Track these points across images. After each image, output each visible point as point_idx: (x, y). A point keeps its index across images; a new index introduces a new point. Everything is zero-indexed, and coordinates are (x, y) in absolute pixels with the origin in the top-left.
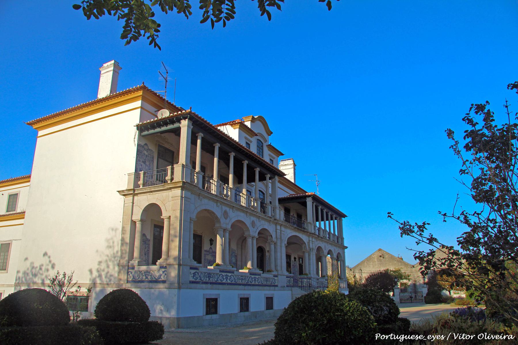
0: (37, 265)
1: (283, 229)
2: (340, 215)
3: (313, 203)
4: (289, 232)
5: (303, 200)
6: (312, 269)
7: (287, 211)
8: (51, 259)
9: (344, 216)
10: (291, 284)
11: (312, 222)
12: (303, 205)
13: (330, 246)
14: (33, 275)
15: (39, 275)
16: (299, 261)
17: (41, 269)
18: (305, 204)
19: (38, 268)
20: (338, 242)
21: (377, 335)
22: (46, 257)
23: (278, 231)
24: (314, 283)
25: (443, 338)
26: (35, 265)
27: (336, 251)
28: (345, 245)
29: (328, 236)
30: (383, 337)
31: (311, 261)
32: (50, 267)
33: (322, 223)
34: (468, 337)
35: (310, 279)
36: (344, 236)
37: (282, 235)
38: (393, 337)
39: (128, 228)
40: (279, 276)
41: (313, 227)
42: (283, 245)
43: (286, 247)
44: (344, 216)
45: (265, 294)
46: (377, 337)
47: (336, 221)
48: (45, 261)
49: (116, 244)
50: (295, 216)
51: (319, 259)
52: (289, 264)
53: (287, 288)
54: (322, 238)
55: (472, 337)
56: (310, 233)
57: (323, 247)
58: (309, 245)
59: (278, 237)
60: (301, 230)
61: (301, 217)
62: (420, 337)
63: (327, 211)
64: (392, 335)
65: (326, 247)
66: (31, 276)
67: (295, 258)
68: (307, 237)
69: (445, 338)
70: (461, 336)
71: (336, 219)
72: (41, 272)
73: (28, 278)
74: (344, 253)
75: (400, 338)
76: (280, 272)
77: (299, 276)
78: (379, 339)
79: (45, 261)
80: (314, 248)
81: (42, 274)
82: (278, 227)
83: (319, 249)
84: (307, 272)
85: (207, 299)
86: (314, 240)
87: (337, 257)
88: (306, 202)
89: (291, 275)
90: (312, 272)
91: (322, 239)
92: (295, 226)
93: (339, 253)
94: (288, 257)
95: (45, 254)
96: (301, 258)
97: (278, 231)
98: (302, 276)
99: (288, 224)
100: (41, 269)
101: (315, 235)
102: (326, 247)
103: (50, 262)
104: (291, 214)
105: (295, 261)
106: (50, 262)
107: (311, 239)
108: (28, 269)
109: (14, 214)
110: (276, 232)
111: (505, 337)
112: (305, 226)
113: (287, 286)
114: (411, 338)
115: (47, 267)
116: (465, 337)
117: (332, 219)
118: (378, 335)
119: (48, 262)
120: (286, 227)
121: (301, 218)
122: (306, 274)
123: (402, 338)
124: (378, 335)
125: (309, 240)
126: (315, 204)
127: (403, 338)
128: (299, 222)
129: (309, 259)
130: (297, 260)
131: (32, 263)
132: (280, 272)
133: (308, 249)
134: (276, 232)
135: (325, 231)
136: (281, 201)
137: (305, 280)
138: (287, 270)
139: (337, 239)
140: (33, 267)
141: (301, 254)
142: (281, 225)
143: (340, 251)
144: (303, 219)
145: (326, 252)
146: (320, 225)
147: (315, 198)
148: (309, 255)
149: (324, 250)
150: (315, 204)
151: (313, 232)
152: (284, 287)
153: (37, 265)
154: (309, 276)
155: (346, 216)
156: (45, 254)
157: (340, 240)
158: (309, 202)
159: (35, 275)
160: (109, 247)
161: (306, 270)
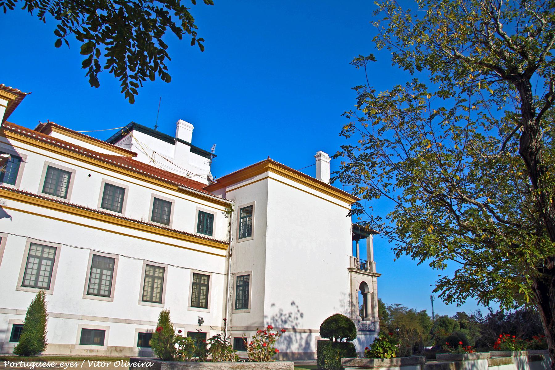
0: (286, 312)
8: (299, 308)
14: (282, 321)
15: (289, 322)
17: (290, 316)
19: (287, 316)
22: (294, 306)
26: (284, 313)
32: (299, 316)
39: (357, 293)
45: (136, 329)
46: (5, 365)
48: (293, 309)
49: (345, 304)
55: (108, 364)
66: (280, 322)
69: (79, 366)
70: (96, 364)
72: (290, 319)
73: (277, 324)
75: (30, 365)
79: (293, 309)
81: (292, 322)
85: (105, 331)
95: (293, 303)
100: (290, 316)
103: (298, 311)
106: (298, 311)
108: (276, 315)
109: (118, 217)
115: (296, 316)
116: (100, 364)
119: (296, 311)
123: (33, 365)
127: (34, 365)
131: (281, 310)
140: (281, 315)
153: (286, 312)
156: (293, 303)
159: (285, 322)
160: (342, 306)
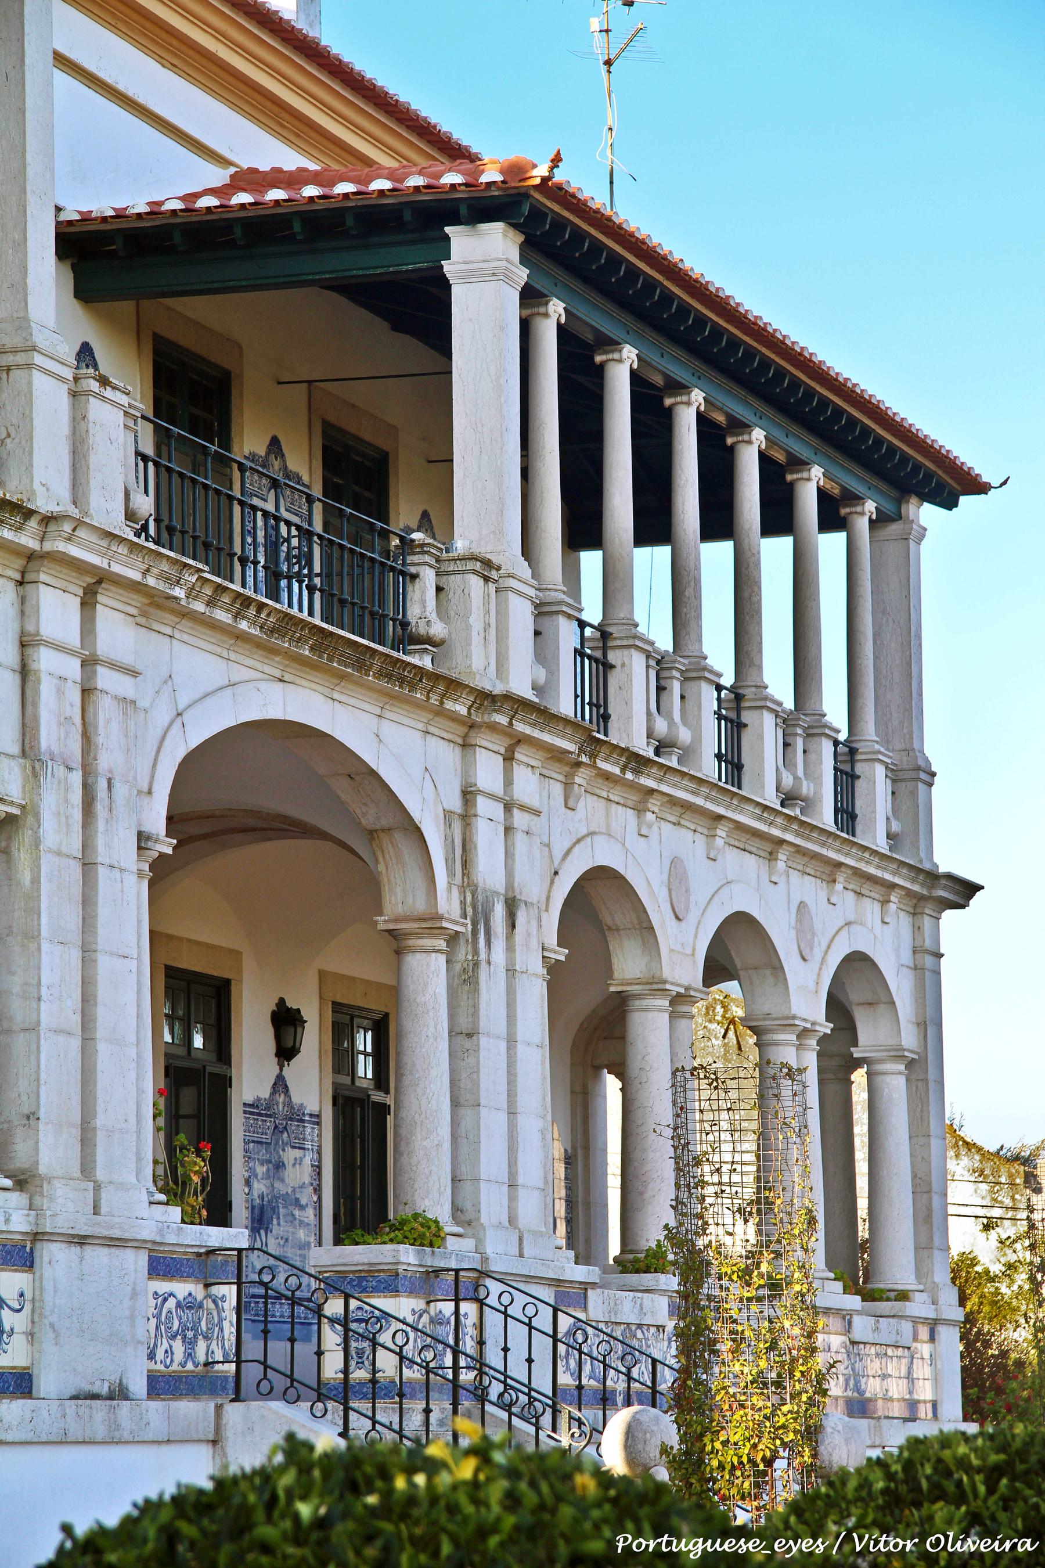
1: (116, 630)
2: (904, 473)
3: (531, 297)
4: (202, 684)
5: (408, 260)
6: (491, 1160)
7: (190, 401)
9: (949, 482)
10: (217, 1349)
11: (508, 552)
12: (399, 324)
13: (745, 865)
16: (343, 1059)
18: (423, 312)
20: (847, 815)
21: (621, 1538)
23: (45, 660)
24: (522, 1355)
25: (822, 1548)
27: (816, 925)
28: (948, 858)
29: (710, 737)
30: (639, 1546)
31: (491, 1052)
33: (652, 564)
34: (896, 1546)
35: (468, 1285)
36: (935, 747)
37: (105, 709)
38: (669, 1544)
40: (55, 1257)
41: (521, 615)
42: (118, 847)
43: (161, 874)
44: (949, 482)
46: (620, 1545)
47: (831, 547)
50: (303, 464)
51: (594, 1037)
52: (194, 1100)
53: (156, 1413)
54: (637, 762)
56: (485, 699)
57: (648, 882)
58: (465, 857)
59: (48, 737)
60: (361, 659)
61: (373, 480)
62: (750, 1545)
63: (728, 413)
64: (666, 1538)
65: (689, 881)
67: (286, 1021)
68: (445, 755)
71: (832, 518)
74: (927, 960)
75: (690, 1547)
76: (65, 1206)
77: (330, 1256)
78: (627, 1549)
80: (531, 884)
82: (57, 609)
83: (598, 905)
84: (436, 1205)
86: (527, 784)
87: (837, 1007)
88: (445, 286)
89: (215, 1236)
90: (491, 1205)
91: (641, 774)
92: (300, 603)
93: (857, 963)
94: (193, 995)
96: (370, 1022)
97: (54, 667)
98: (359, 1255)
99: (187, 582)
101: (546, 716)
102: (689, 881)
104: (249, 442)
105: (286, 1053)
107: (488, 770)
110: (24, 672)
111: (1008, 1545)
112: (421, 605)
113: (160, 1386)
114: (726, 1546)
116: (886, 1543)
117: (779, 518)
118: (626, 1539)
120: (153, 606)
121: (381, 509)
122: (427, 1234)
124: (626, 1539)
125: (468, 795)
126: (557, 308)
128: (352, 542)
129: (463, 1034)
130: (313, 1040)
132: (65, 1206)
133: (449, 903)
134: (24, 672)
135: (676, 667)
136: (103, 256)
137: (404, 1306)
138: (172, 1185)
139: (846, 779)
141: (355, 964)
142: (94, 586)
143: (883, 936)
144: (404, 514)
145: (681, 950)
146: (616, 585)
147: (573, 247)
148: (465, 981)
149: (658, 913)
150: (557, 308)
151: (520, 683)
152: (119, 1393)
154: (457, 1252)
155: (979, 488)
157: (876, 789)
158: (483, 268)
161: (425, 1184)
